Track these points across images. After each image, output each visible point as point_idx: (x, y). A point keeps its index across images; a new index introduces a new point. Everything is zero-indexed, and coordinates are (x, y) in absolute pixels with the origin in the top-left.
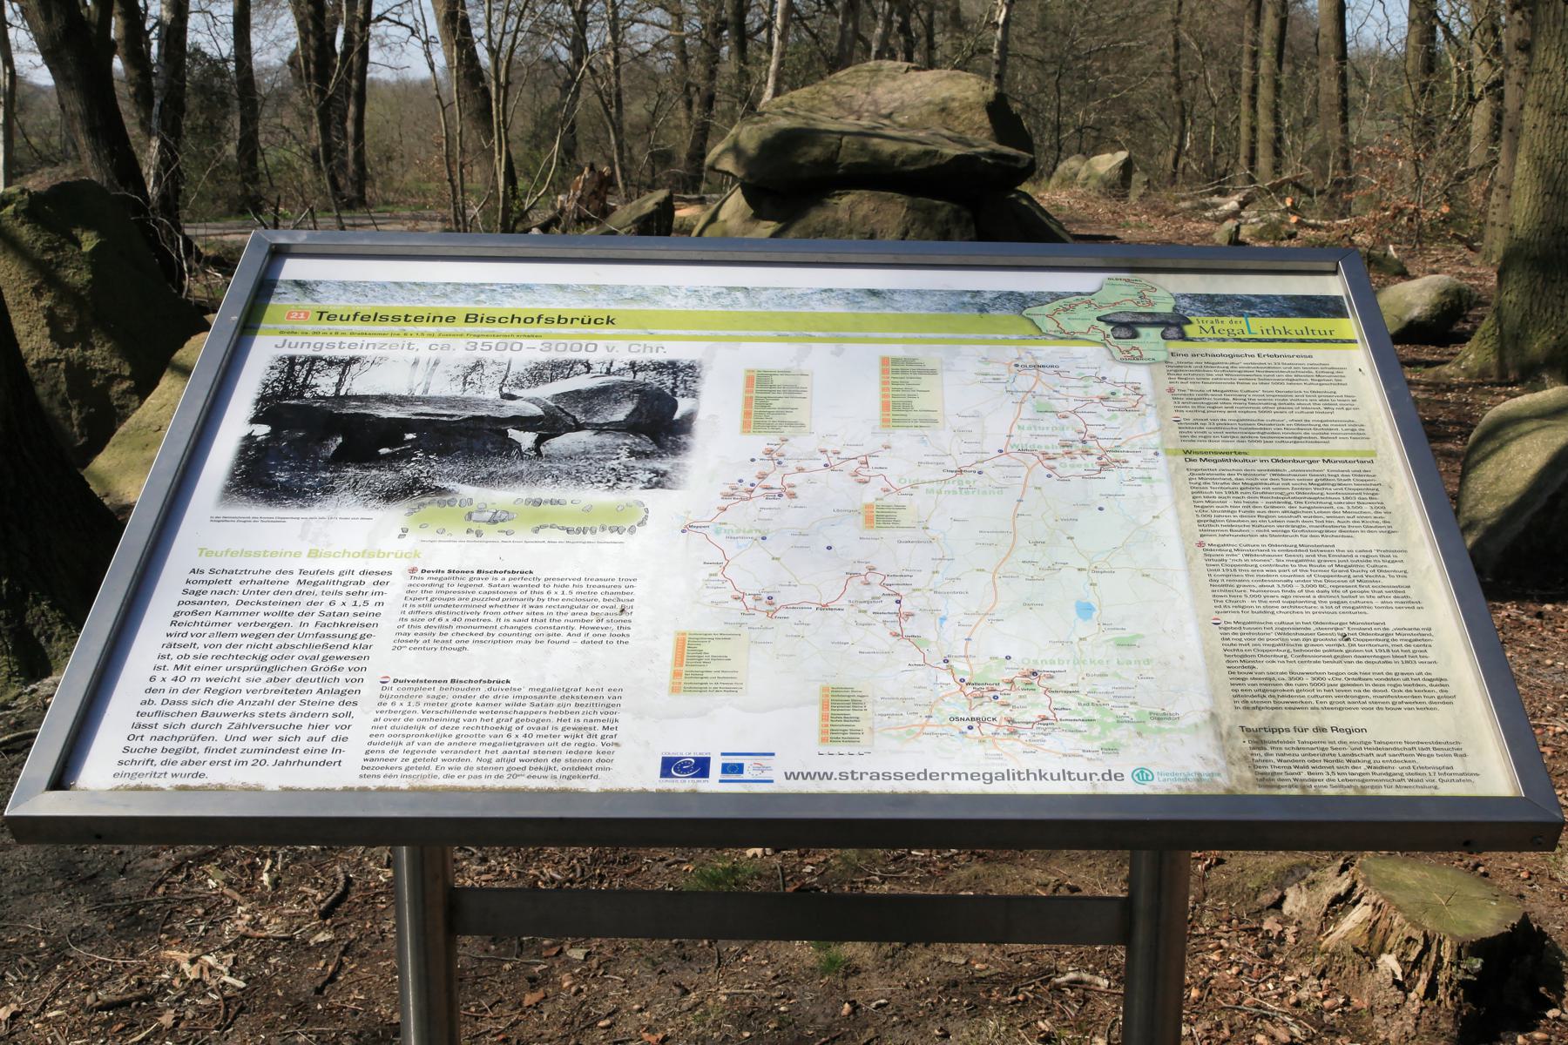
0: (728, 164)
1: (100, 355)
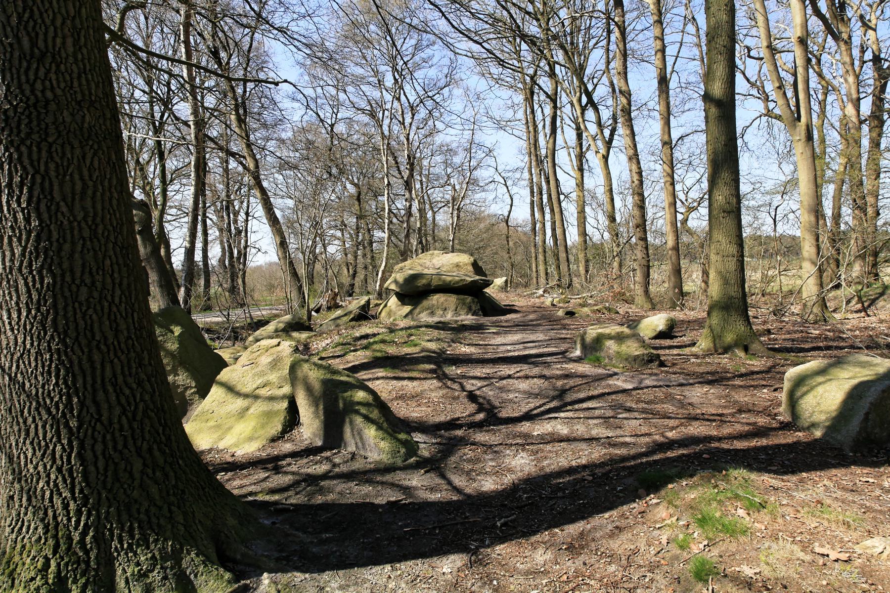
0: (393, 287)
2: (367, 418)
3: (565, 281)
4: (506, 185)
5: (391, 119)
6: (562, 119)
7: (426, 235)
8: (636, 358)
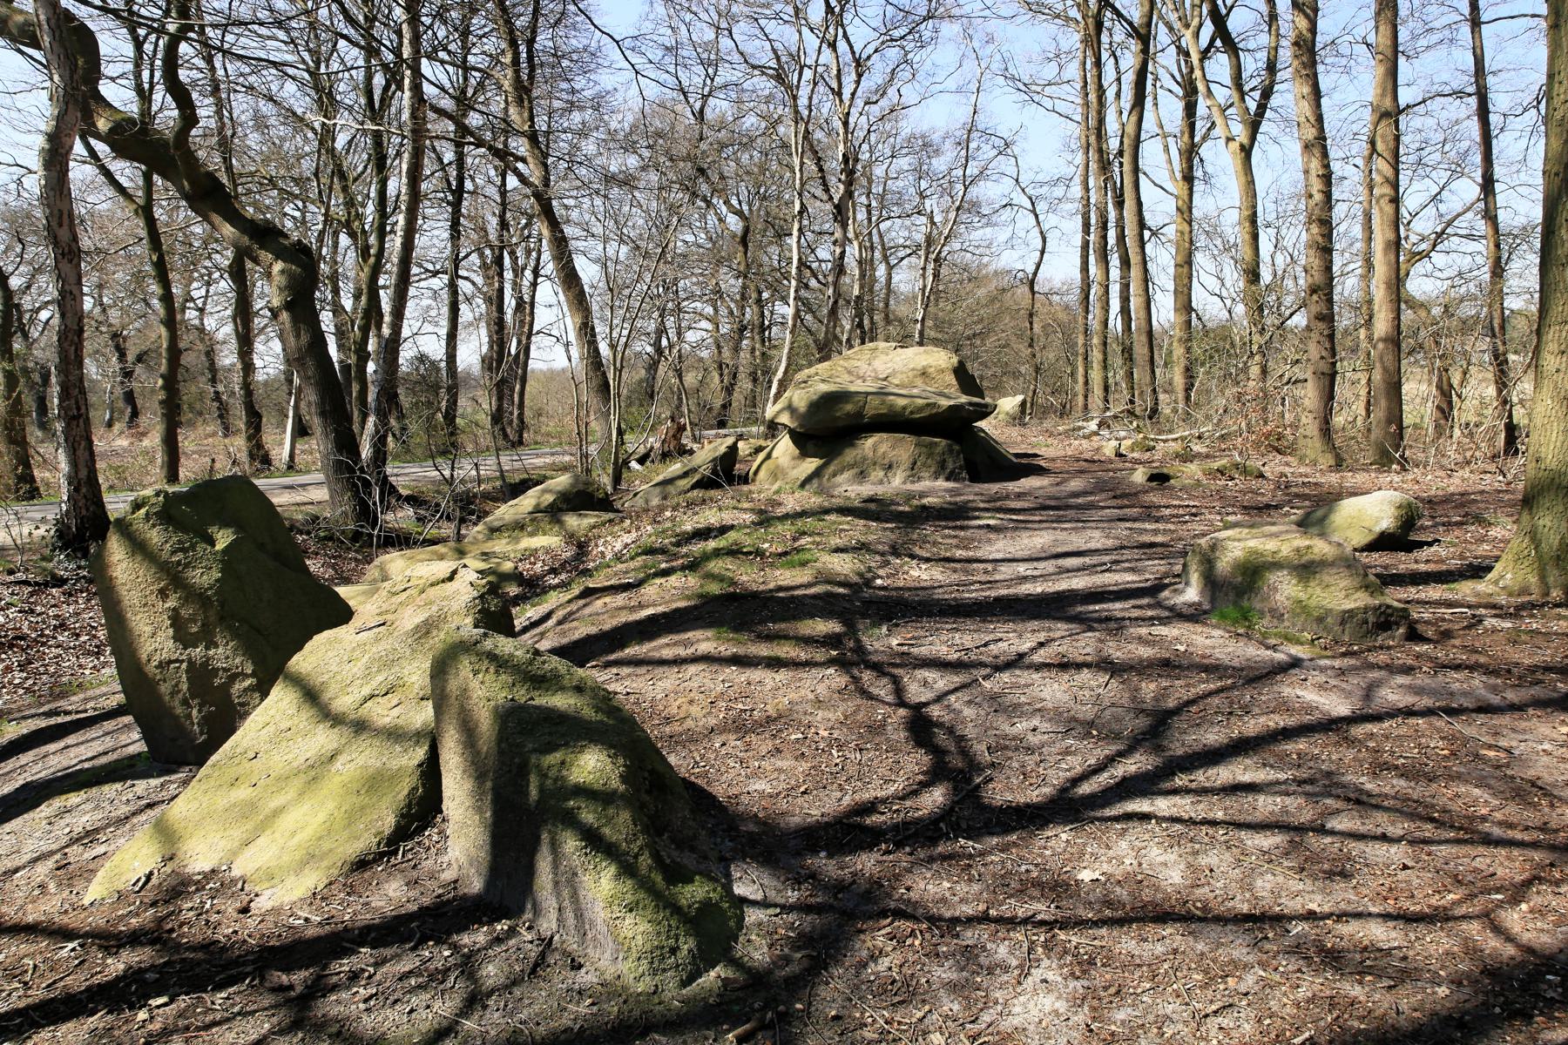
0: (785, 419)
1: (224, 654)
2: (594, 840)
3: (1143, 404)
4: (1034, 211)
5: (815, 84)
6: (1156, 79)
7: (871, 311)
8: (1346, 617)
